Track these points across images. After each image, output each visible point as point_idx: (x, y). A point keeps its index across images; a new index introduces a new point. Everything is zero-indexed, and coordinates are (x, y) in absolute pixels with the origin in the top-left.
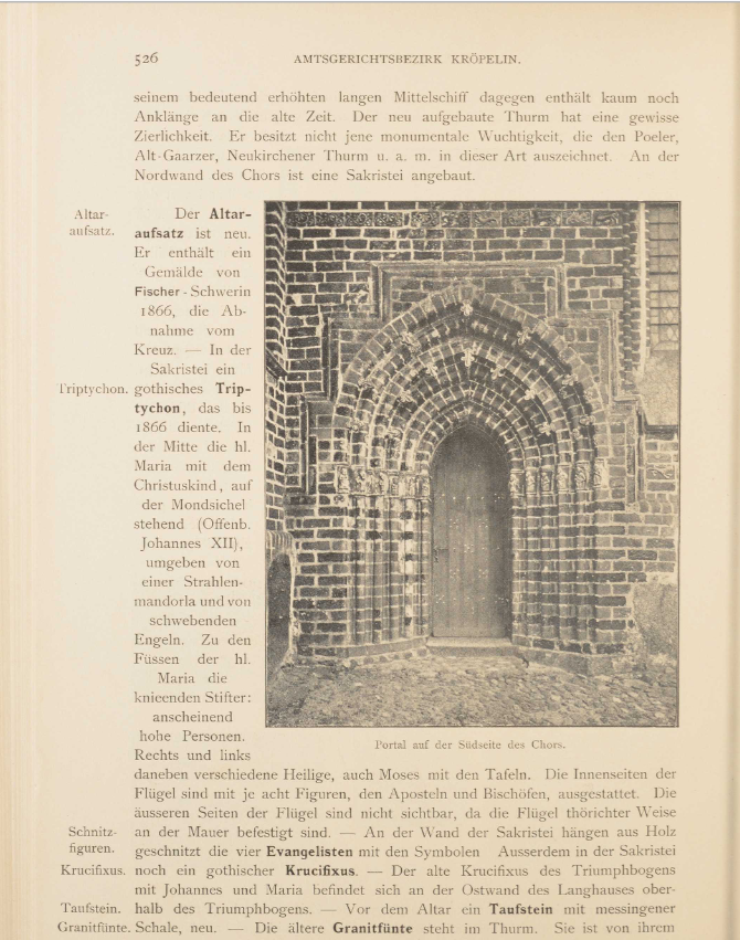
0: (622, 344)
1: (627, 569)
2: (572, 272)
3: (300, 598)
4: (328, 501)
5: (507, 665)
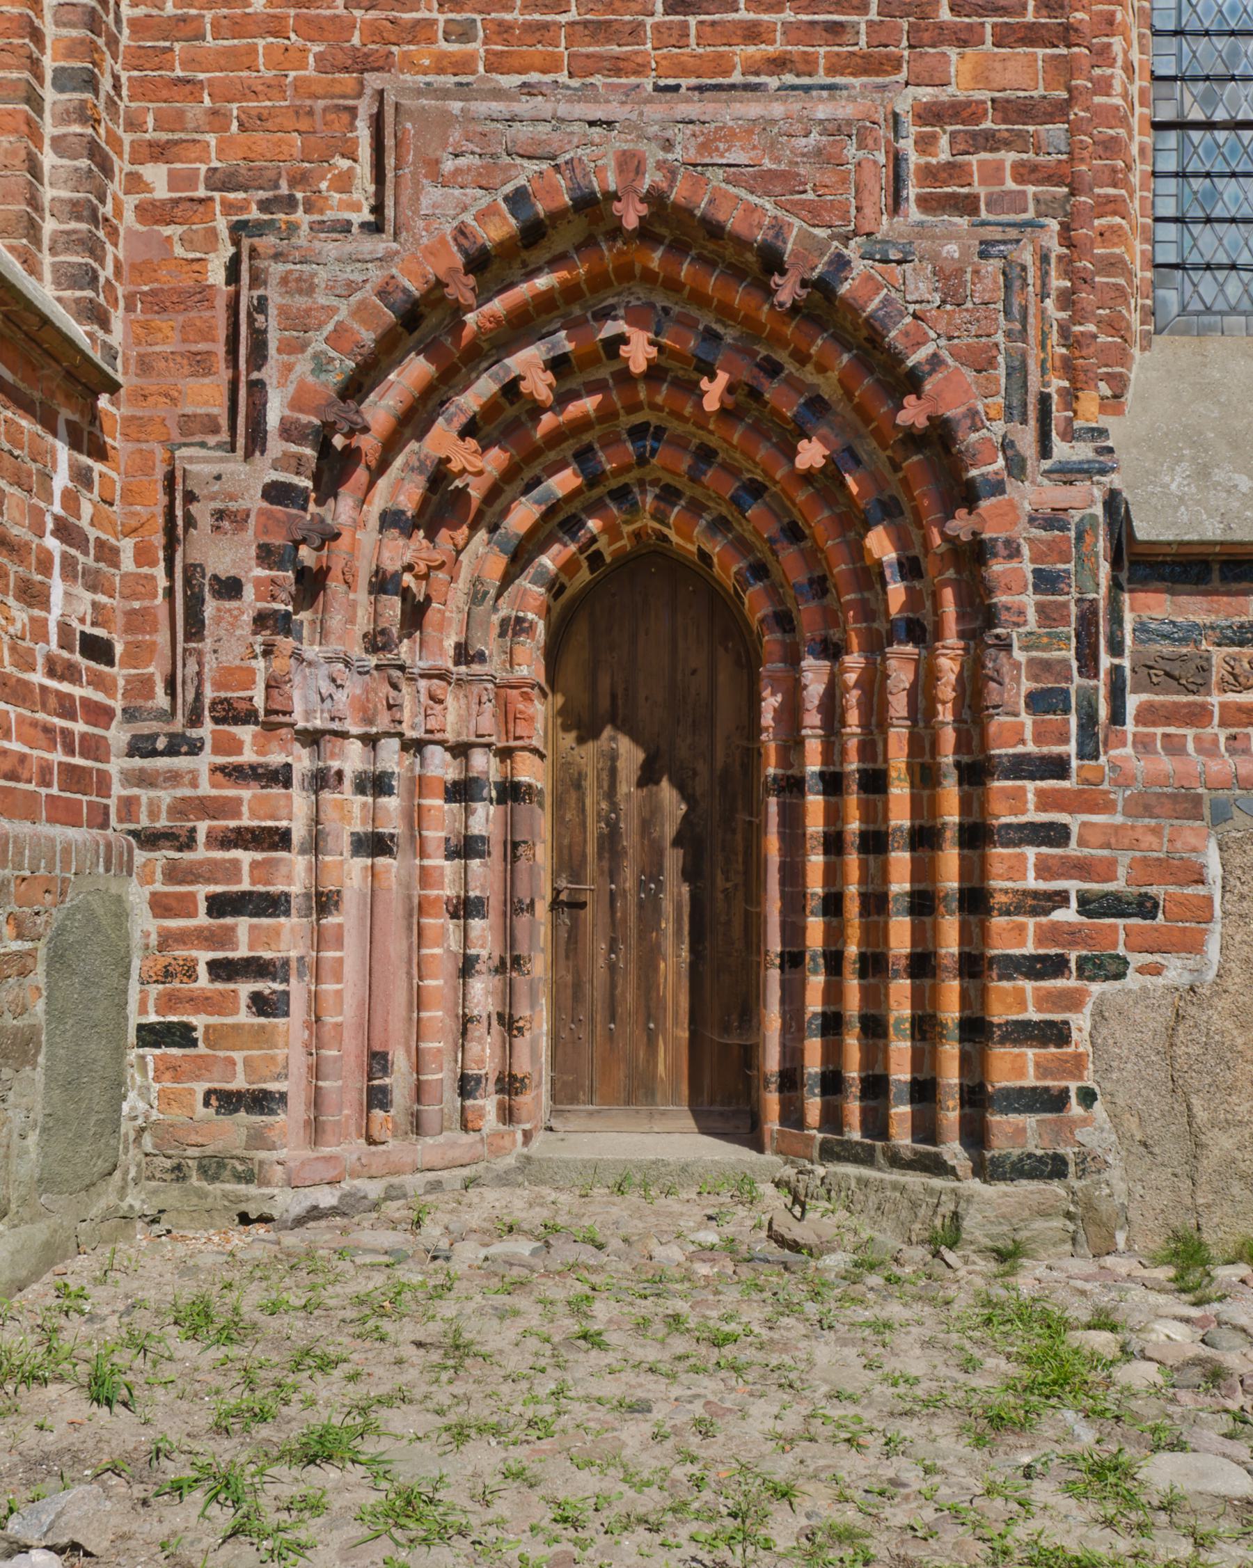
0: (1064, 315)
1: (1073, 944)
2: (932, 115)
3: (153, 1018)
4: (235, 746)
5: (1147, 1101)
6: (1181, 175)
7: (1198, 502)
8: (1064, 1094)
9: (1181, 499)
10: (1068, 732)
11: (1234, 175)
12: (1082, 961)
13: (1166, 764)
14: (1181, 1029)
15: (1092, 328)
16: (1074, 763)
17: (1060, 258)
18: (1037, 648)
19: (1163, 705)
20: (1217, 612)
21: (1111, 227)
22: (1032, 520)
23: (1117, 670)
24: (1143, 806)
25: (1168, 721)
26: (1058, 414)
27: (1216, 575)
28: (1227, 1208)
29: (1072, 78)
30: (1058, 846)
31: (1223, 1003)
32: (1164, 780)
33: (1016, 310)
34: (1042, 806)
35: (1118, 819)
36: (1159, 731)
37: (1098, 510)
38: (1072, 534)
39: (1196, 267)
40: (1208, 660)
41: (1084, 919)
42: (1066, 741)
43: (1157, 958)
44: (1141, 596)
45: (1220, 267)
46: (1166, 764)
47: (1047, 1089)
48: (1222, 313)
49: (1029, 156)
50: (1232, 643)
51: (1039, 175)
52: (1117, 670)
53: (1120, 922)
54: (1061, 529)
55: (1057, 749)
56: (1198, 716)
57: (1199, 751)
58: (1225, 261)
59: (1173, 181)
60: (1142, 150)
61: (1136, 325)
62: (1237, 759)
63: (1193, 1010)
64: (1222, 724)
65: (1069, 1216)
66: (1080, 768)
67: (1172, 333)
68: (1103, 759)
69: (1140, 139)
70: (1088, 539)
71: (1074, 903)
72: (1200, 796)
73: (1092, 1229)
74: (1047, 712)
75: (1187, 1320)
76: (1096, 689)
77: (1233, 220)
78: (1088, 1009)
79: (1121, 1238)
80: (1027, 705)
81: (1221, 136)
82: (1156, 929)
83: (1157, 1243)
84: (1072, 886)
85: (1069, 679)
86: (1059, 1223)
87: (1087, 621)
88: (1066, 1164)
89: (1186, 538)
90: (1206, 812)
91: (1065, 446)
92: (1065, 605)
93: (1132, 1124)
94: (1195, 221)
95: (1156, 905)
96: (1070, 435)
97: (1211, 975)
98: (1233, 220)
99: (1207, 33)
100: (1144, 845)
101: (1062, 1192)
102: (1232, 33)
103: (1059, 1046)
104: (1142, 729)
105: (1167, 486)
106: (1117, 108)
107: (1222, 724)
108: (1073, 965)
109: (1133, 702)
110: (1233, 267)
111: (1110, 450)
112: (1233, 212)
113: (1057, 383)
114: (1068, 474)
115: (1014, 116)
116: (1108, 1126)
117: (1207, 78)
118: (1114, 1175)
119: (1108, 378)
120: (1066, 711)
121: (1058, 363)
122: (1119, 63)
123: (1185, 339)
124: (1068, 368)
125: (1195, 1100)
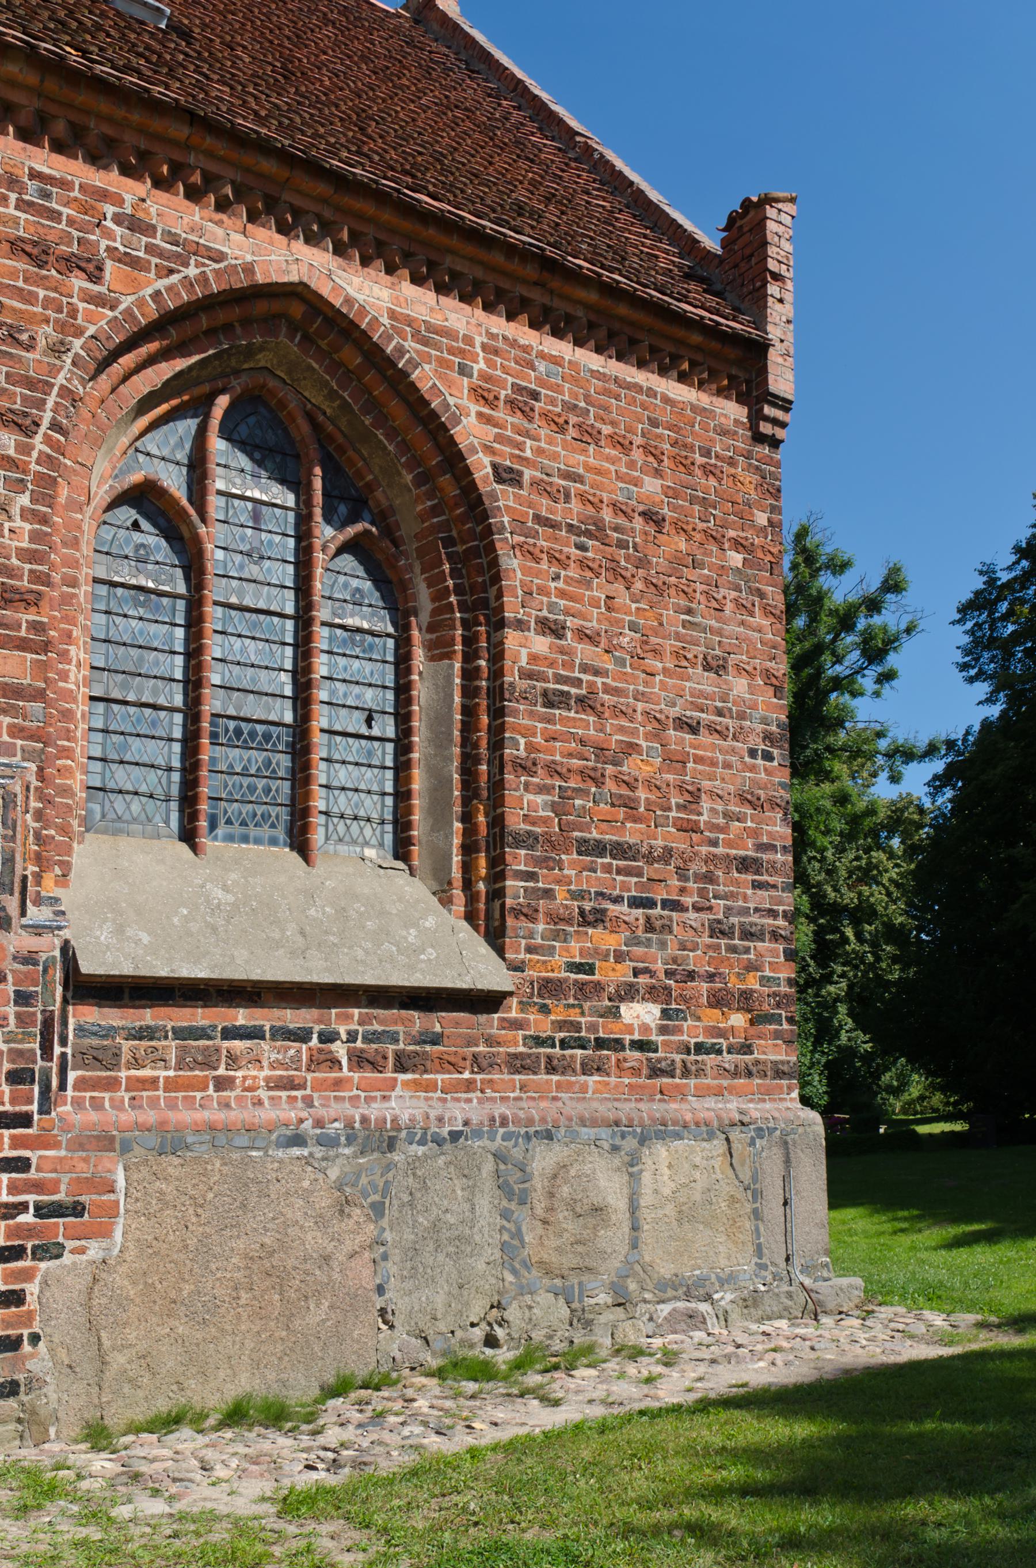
0: (37, 825)
1: (29, 1237)
5: (73, 1338)
6: (105, 731)
7: (118, 950)
8: (19, 1339)
9: (107, 947)
10: (32, 1097)
11: (138, 735)
12: (35, 1248)
13: (93, 1116)
14: (96, 1288)
15: (53, 832)
16: (36, 1117)
17: (37, 788)
18: (15, 1042)
19: (91, 1078)
20: (126, 1019)
21: (65, 766)
22: (15, 958)
23: (64, 1055)
24: (78, 1144)
25: (94, 1088)
26: (31, 888)
27: (126, 995)
28: (120, 1403)
29: (46, 672)
30: (23, 1172)
31: (123, 1269)
32: (92, 1127)
33: (10, 822)
34: (13, 1146)
35: (63, 1153)
36: (88, 1094)
37: (57, 953)
38: (41, 968)
39: (113, 791)
40: (120, 1049)
41: (38, 1220)
42: (31, 1103)
43: (83, 1242)
44: (80, 1007)
45: (128, 792)
46: (93, 1116)
47: (8, 1337)
48: (127, 822)
49: (20, 721)
50: (135, 1038)
51: (25, 734)
52: (64, 1055)
53: (61, 1220)
54: (34, 965)
55: (25, 1108)
56: (112, 1084)
57: (112, 1107)
58: (131, 789)
59: (101, 734)
60: (83, 715)
61: (76, 828)
62: (137, 1112)
63: (104, 1275)
64: (127, 1090)
65: (19, 1421)
66: (40, 1120)
67: (96, 832)
68: (53, 1114)
69: (81, 708)
70: (50, 971)
71: (31, 1210)
72: (114, 1136)
73: (34, 1428)
74: (19, 1084)
75: (110, 1460)
76: (51, 1068)
77: (137, 764)
78: (37, 1280)
79: (52, 1431)
80: (7, 1079)
81: (132, 710)
82: (83, 1224)
83: (76, 1431)
84: (31, 1198)
85: (35, 1062)
86: (12, 1426)
87: (47, 1024)
88: (19, 1385)
89: (112, 973)
90: (117, 1146)
91: (35, 909)
92: (34, 1014)
93: (62, 1354)
94: (113, 761)
95: (84, 1208)
96: (38, 901)
97: (116, 1252)
98: (137, 764)
99: (124, 644)
100: (78, 1169)
101: (16, 1405)
102: (140, 647)
103: (17, 1306)
104: (77, 1094)
105: (98, 938)
106: (72, 691)
107: (127, 1090)
108: (29, 1251)
109: (72, 1076)
110: (136, 793)
111: (63, 913)
112: (137, 758)
113: (32, 868)
114: (38, 930)
115: (10, 694)
116: (47, 1357)
117: (124, 672)
118: (50, 1390)
119: (61, 863)
120: (32, 1082)
121: (32, 856)
122: (74, 662)
123: (105, 837)
124: (38, 859)
125: (103, 1334)
